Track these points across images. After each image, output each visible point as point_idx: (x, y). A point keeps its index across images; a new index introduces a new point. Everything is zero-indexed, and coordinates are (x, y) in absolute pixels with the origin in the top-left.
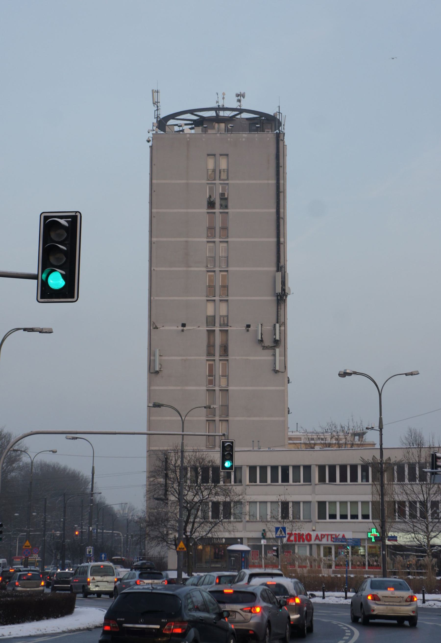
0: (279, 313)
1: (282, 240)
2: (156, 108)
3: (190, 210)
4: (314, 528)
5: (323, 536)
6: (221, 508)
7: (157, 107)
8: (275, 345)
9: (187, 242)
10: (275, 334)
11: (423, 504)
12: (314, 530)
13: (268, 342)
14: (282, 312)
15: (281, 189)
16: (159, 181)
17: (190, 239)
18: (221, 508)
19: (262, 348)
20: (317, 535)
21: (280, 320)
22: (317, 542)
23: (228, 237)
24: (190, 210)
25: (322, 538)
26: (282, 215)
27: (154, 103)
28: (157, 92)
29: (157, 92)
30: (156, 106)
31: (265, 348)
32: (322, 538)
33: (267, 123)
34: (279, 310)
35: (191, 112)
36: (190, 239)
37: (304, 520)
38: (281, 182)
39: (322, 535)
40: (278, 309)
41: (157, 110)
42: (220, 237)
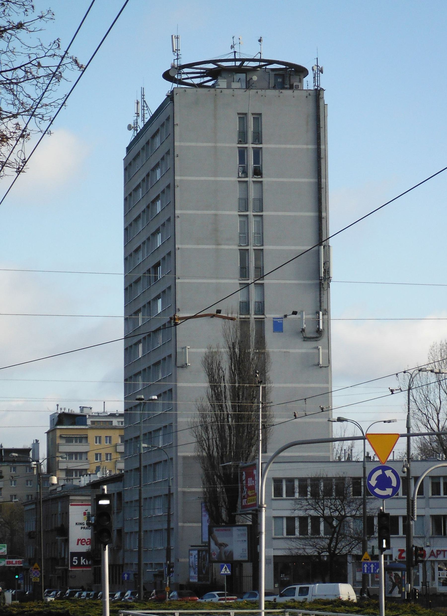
0: (322, 299)
1: (324, 214)
2: (176, 57)
3: (212, 179)
4: (428, 544)
5: (439, 552)
6: (297, 524)
7: (178, 55)
8: (318, 336)
9: (216, 215)
10: (319, 325)
11: (303, 520)
12: (428, 546)
13: (310, 333)
14: (324, 299)
15: (322, 155)
16: (182, 144)
17: (220, 212)
18: (297, 524)
19: (303, 340)
20: (432, 551)
21: (321, 307)
22: (432, 558)
23: (262, 211)
24: (212, 179)
25: (438, 554)
26: (323, 186)
27: (173, 51)
28: (177, 38)
29: (177, 38)
30: (176, 54)
31: (306, 339)
32: (438, 554)
33: (289, 75)
34: (322, 295)
35: (214, 62)
36: (220, 212)
37: (416, 536)
38: (322, 147)
39: (437, 551)
40: (320, 294)
41: (177, 59)
42: (254, 210)
